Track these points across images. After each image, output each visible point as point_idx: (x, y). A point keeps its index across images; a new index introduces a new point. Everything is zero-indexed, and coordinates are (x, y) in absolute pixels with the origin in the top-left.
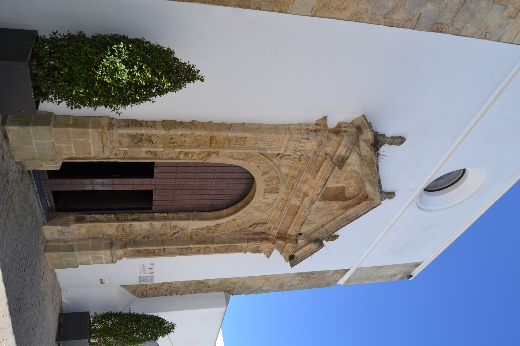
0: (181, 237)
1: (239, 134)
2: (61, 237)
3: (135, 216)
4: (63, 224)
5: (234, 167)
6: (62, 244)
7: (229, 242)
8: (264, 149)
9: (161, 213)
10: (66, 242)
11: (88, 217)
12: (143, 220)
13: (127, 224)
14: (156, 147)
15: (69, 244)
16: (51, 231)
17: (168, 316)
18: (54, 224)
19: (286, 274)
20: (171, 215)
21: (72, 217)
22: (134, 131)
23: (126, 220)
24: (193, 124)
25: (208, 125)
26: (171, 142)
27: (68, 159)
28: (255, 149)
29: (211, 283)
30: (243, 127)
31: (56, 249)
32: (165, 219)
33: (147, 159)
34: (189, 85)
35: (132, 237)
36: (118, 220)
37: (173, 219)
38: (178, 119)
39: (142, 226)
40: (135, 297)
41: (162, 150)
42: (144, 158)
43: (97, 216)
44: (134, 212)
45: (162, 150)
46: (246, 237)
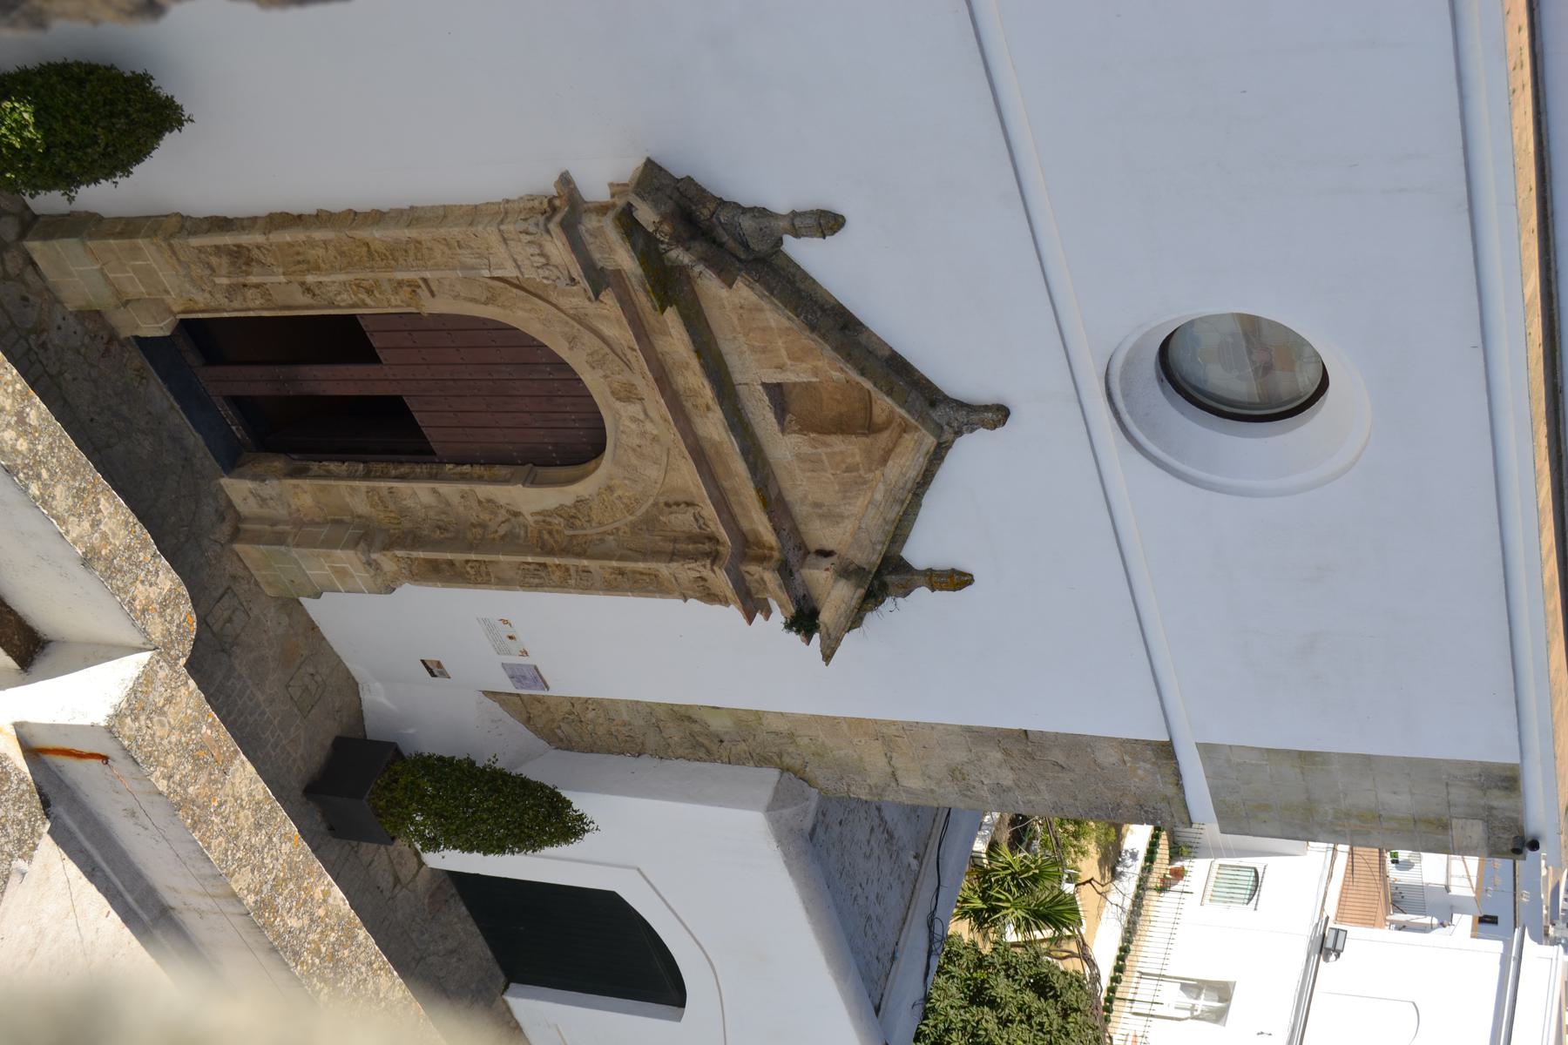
0: (518, 537)
1: (406, 234)
2: (265, 512)
3: (404, 469)
4: (254, 478)
5: (485, 321)
6: (267, 527)
7: (622, 558)
8: (473, 268)
9: (457, 464)
10: (274, 523)
11: (315, 466)
12: (417, 478)
13: (384, 485)
14: (273, 274)
15: (280, 528)
16: (240, 490)
17: (580, 802)
18: (241, 476)
19: (932, 727)
20: (478, 470)
21: (279, 463)
22: (227, 239)
23: (384, 476)
24: (322, 218)
25: (352, 218)
26: (299, 261)
27: (183, 312)
28: (454, 269)
29: (717, 724)
30: (412, 216)
31: (256, 539)
32: (463, 478)
33: (307, 307)
34: (170, 140)
35: (407, 525)
36: (367, 476)
37: (481, 479)
38: (295, 211)
39: (419, 495)
40: (542, 743)
41: (282, 279)
42: (307, 307)
43: (333, 466)
44: (403, 458)
45: (282, 279)
46: (669, 547)
